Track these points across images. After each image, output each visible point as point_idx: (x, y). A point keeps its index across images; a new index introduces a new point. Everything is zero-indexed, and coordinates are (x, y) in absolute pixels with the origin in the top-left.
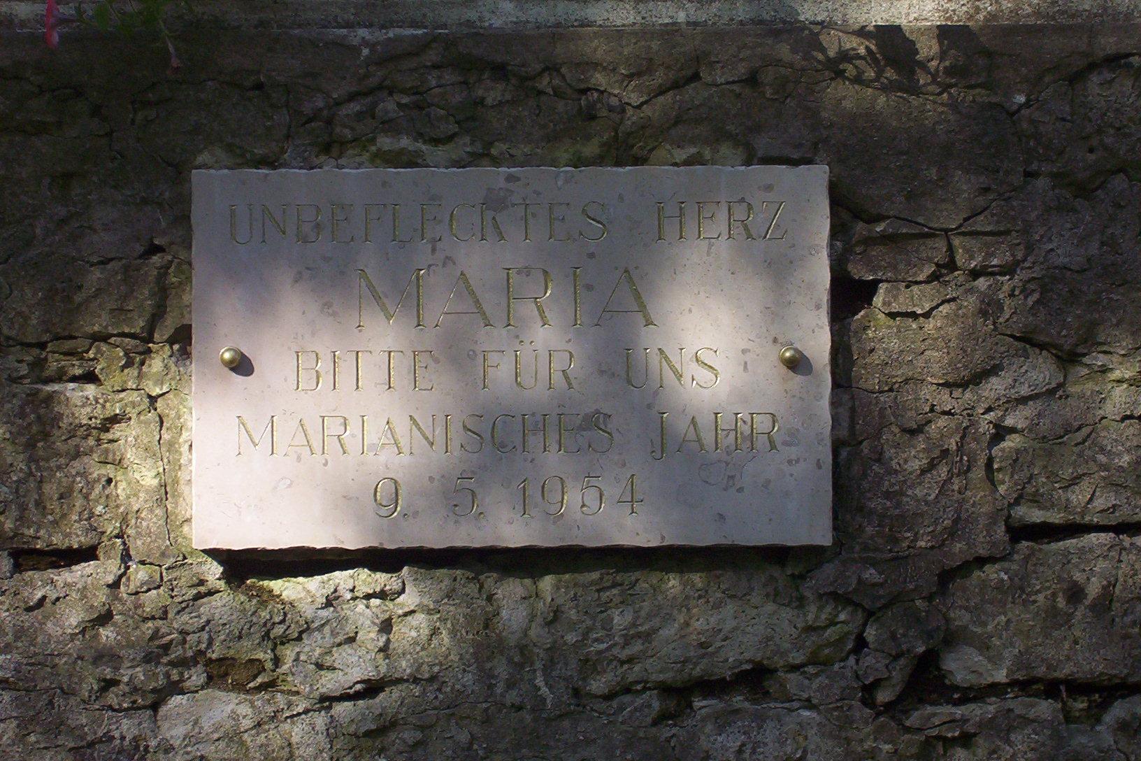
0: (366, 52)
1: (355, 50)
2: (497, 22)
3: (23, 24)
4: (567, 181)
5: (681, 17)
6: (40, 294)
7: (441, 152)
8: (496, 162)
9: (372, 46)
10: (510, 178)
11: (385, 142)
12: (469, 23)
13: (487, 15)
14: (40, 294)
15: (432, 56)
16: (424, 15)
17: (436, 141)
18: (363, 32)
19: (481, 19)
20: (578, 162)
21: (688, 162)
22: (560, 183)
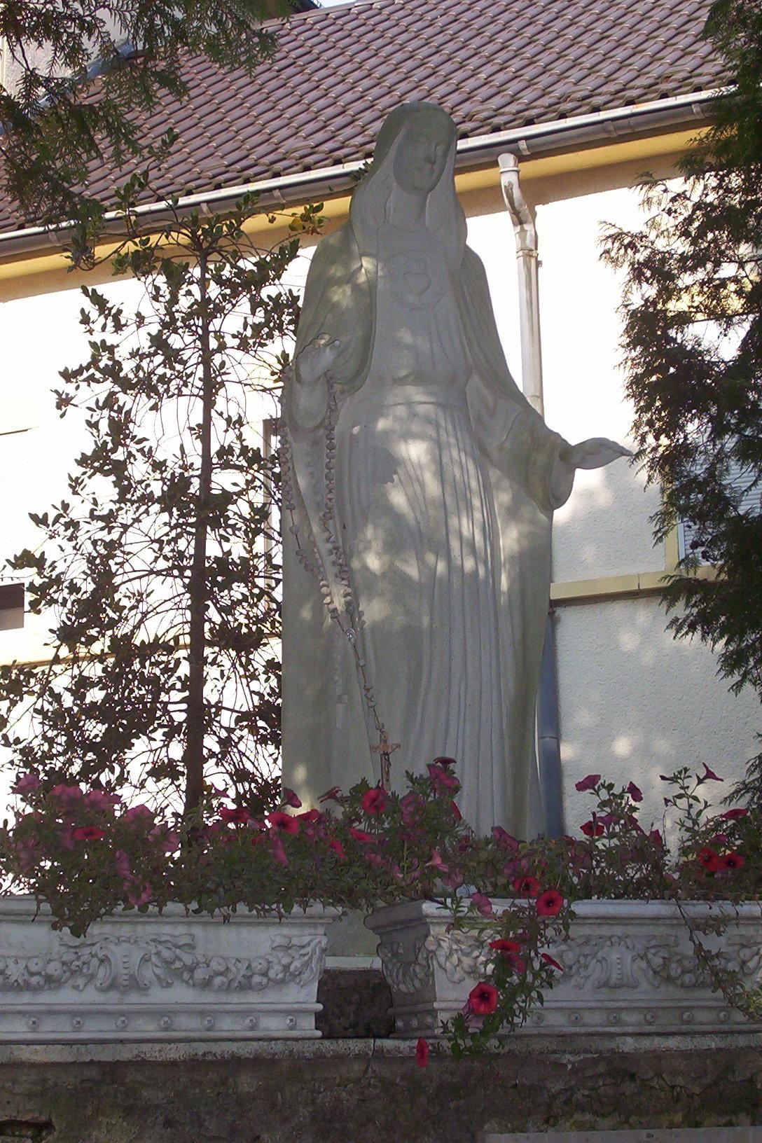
0: (570, 1067)
1: (565, 1066)
2: (626, 1050)
3: (389, 1052)
4: (676, 1136)
5: (713, 1045)
6: (723, 619)
7: (606, 1123)
8: (632, 1127)
9: (573, 1064)
10: (649, 1136)
11: (578, 1117)
12: (612, 1050)
13: (621, 1046)
14: (723, 619)
15: (601, 1068)
16: (591, 1046)
17: (603, 1116)
18: (568, 1056)
19: (618, 1047)
20: (672, 1126)
21: (725, 1125)
22: (673, 1137)
